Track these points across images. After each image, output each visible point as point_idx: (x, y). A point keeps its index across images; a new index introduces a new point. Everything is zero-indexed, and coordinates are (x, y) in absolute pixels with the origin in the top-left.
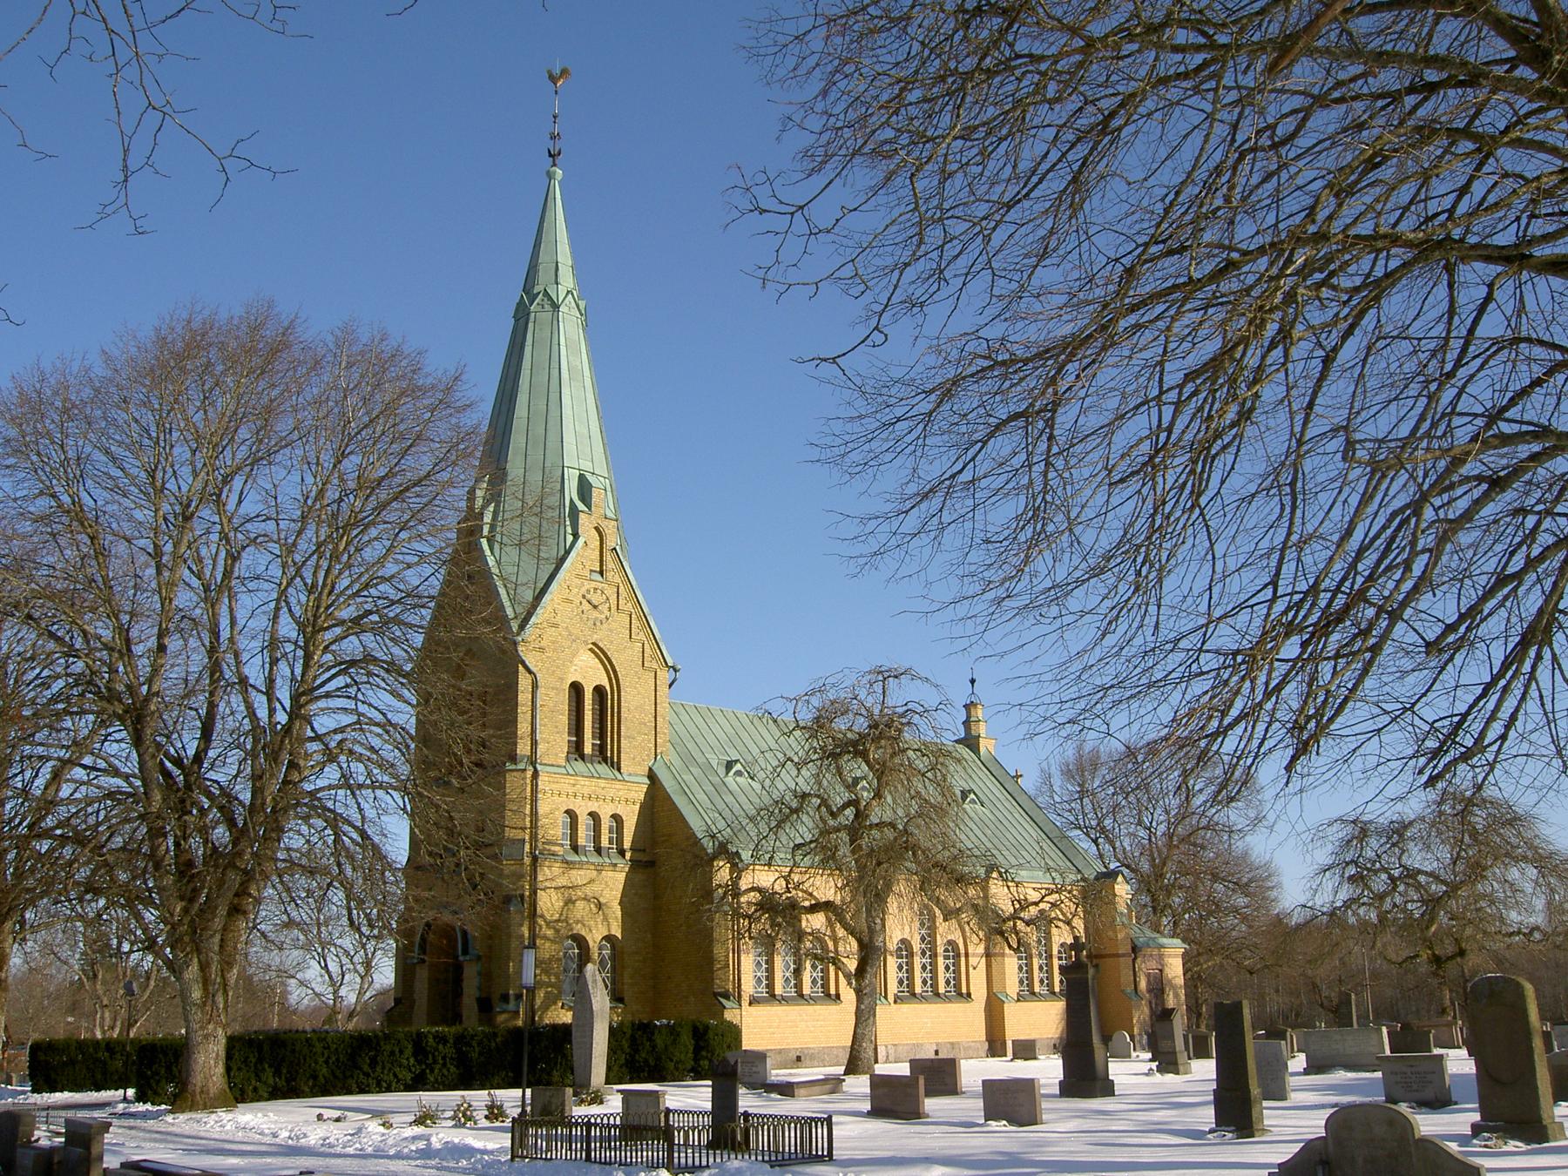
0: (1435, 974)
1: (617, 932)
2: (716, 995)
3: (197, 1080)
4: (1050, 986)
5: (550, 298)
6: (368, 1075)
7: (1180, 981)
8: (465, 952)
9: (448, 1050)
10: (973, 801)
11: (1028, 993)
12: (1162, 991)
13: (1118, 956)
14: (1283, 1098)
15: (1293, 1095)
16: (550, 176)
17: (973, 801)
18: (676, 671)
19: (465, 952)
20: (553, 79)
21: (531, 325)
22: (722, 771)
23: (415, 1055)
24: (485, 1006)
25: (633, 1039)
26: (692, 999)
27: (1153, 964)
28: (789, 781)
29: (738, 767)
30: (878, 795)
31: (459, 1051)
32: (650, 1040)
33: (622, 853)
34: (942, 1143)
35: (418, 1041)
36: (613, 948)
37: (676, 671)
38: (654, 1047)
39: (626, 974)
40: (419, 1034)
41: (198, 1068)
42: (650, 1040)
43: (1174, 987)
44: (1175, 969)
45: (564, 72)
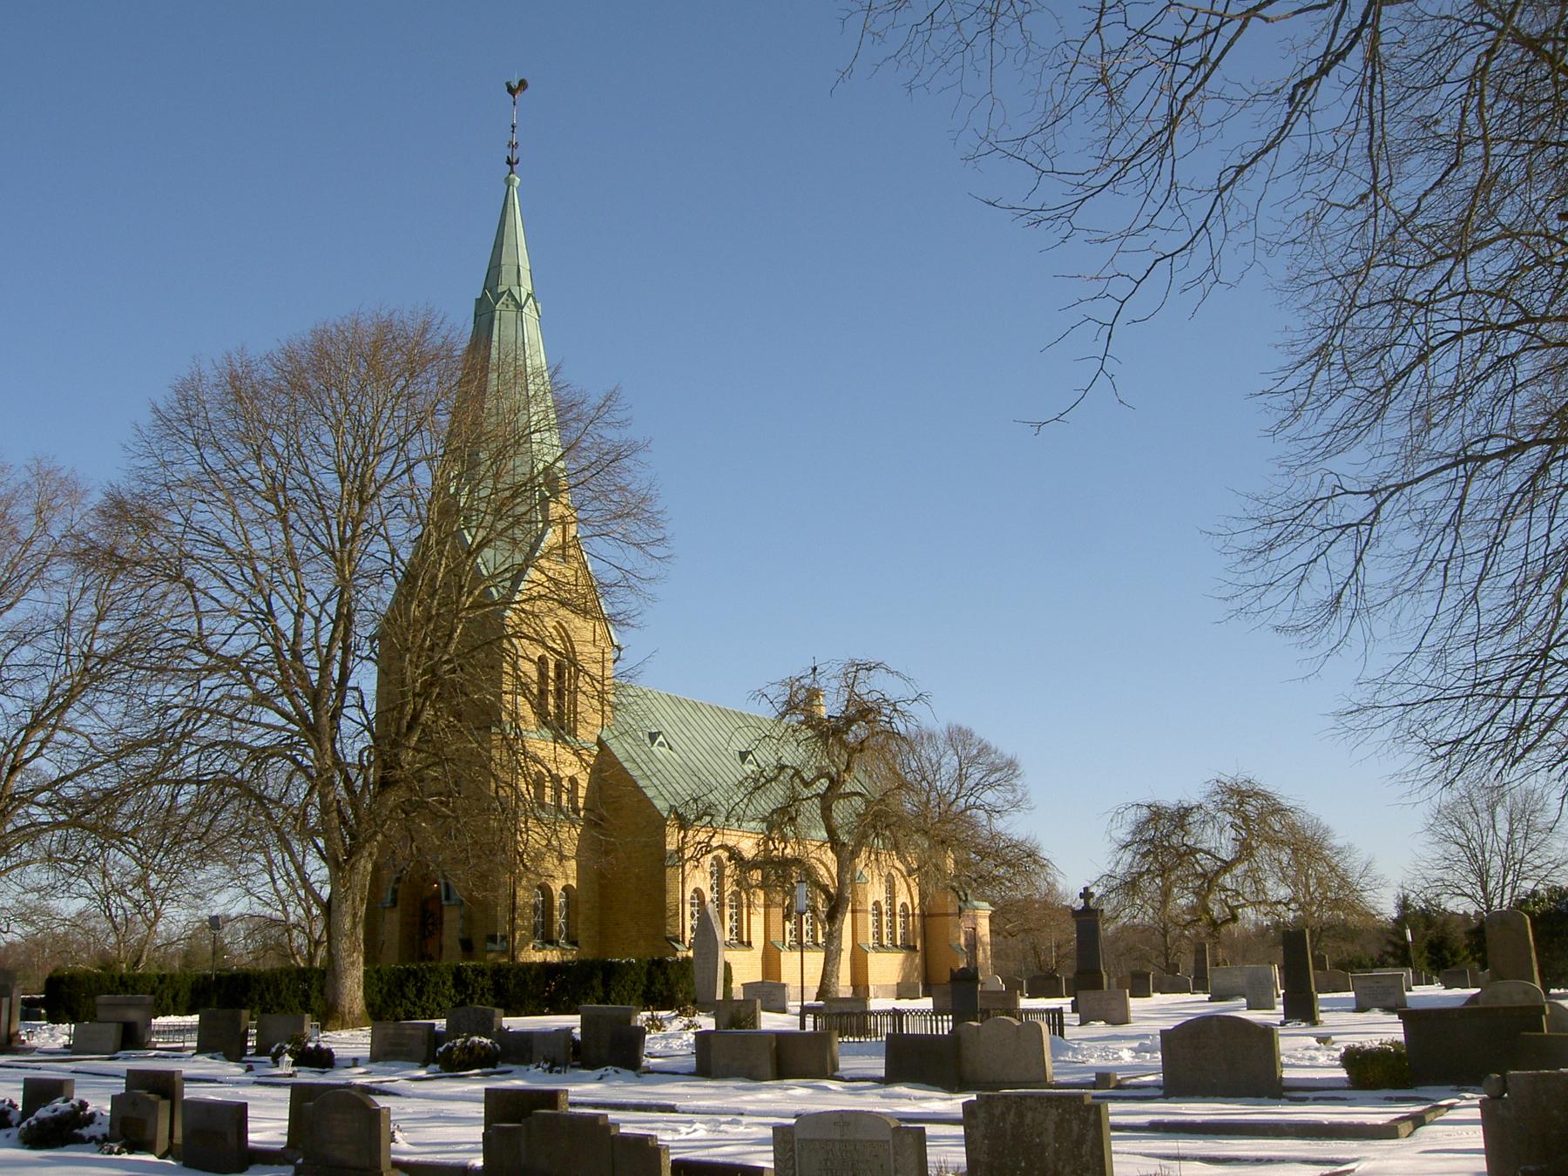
0: (1211, 935)
1: (573, 883)
2: (668, 939)
3: (346, 1002)
4: (893, 939)
5: (514, 299)
6: (414, 1004)
7: (987, 939)
8: (448, 898)
9: (486, 982)
10: (661, 744)
11: (880, 947)
12: (975, 947)
13: (947, 915)
14: (778, 1129)
15: (769, 1132)
16: (509, 182)
17: (661, 744)
18: (620, 649)
19: (448, 898)
20: (512, 91)
21: (496, 322)
22: (647, 741)
23: (455, 986)
24: (467, 946)
25: (649, 974)
26: (642, 942)
27: (970, 924)
28: (765, 757)
29: (661, 738)
30: (848, 768)
31: (496, 983)
32: (664, 973)
33: (576, 810)
34: (764, 1096)
35: (458, 974)
36: (567, 897)
37: (620, 649)
38: (668, 980)
39: (580, 920)
40: (459, 969)
41: (346, 991)
42: (664, 973)
43: (983, 944)
44: (984, 928)
45: (523, 84)
